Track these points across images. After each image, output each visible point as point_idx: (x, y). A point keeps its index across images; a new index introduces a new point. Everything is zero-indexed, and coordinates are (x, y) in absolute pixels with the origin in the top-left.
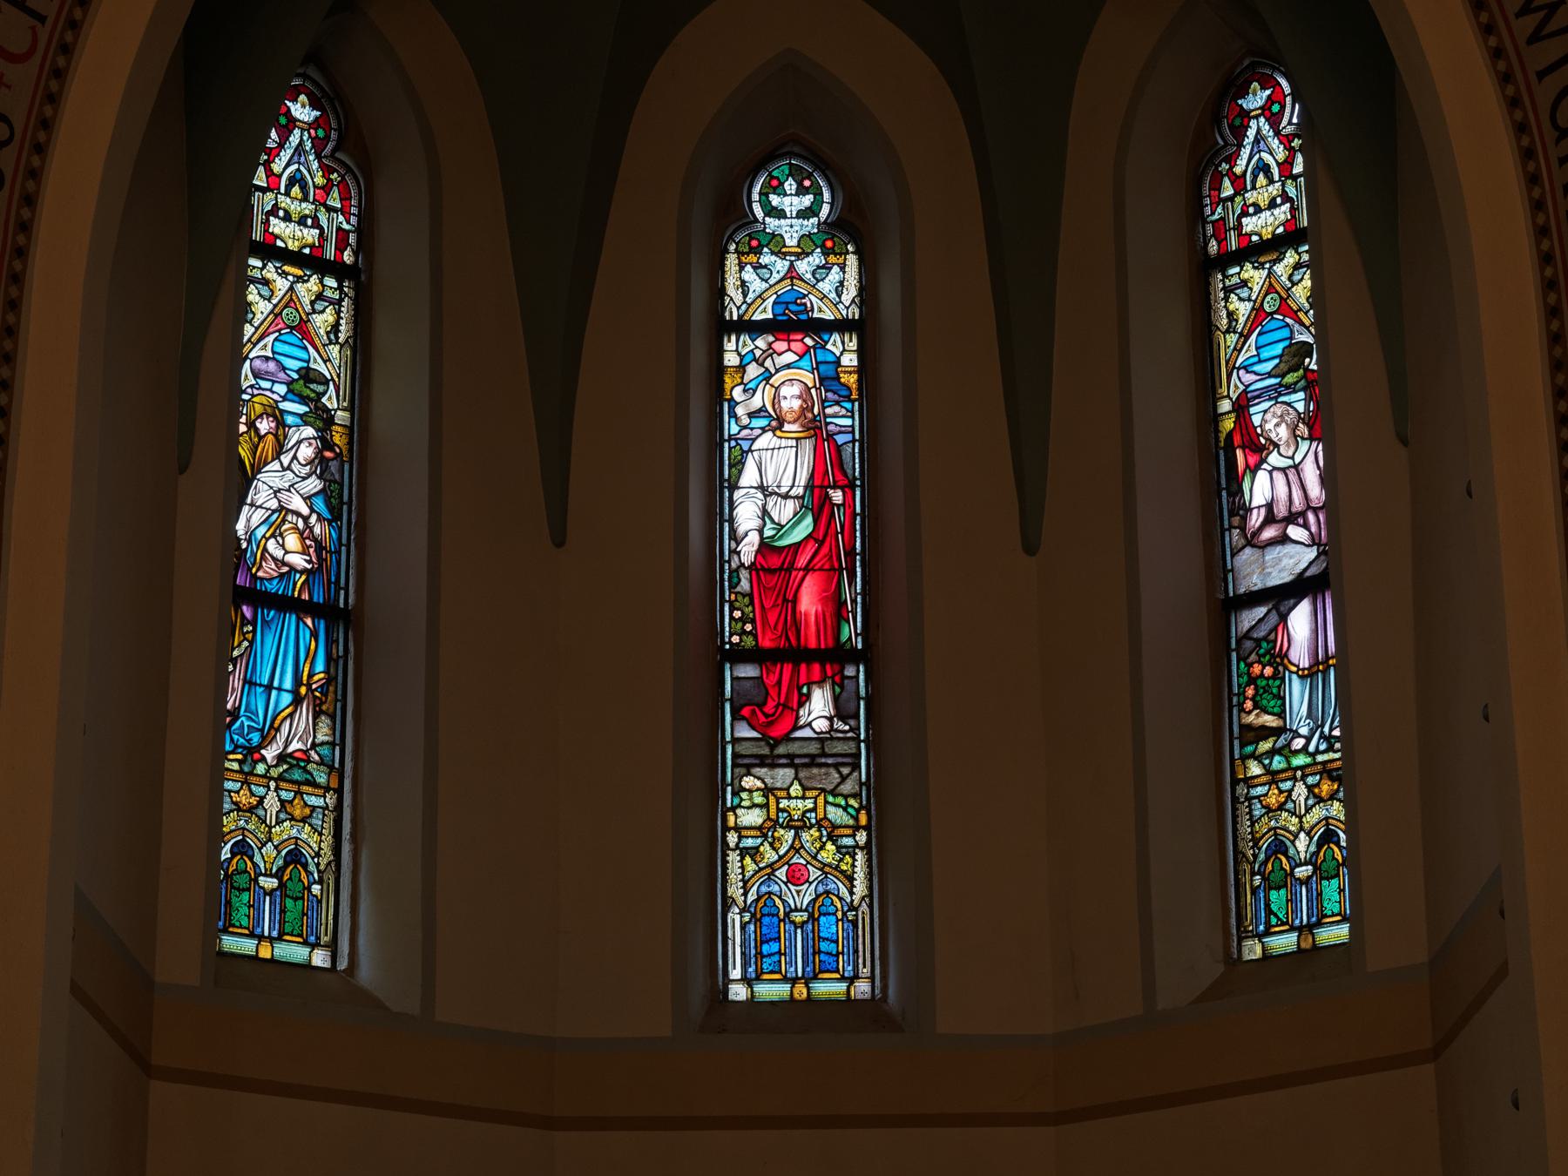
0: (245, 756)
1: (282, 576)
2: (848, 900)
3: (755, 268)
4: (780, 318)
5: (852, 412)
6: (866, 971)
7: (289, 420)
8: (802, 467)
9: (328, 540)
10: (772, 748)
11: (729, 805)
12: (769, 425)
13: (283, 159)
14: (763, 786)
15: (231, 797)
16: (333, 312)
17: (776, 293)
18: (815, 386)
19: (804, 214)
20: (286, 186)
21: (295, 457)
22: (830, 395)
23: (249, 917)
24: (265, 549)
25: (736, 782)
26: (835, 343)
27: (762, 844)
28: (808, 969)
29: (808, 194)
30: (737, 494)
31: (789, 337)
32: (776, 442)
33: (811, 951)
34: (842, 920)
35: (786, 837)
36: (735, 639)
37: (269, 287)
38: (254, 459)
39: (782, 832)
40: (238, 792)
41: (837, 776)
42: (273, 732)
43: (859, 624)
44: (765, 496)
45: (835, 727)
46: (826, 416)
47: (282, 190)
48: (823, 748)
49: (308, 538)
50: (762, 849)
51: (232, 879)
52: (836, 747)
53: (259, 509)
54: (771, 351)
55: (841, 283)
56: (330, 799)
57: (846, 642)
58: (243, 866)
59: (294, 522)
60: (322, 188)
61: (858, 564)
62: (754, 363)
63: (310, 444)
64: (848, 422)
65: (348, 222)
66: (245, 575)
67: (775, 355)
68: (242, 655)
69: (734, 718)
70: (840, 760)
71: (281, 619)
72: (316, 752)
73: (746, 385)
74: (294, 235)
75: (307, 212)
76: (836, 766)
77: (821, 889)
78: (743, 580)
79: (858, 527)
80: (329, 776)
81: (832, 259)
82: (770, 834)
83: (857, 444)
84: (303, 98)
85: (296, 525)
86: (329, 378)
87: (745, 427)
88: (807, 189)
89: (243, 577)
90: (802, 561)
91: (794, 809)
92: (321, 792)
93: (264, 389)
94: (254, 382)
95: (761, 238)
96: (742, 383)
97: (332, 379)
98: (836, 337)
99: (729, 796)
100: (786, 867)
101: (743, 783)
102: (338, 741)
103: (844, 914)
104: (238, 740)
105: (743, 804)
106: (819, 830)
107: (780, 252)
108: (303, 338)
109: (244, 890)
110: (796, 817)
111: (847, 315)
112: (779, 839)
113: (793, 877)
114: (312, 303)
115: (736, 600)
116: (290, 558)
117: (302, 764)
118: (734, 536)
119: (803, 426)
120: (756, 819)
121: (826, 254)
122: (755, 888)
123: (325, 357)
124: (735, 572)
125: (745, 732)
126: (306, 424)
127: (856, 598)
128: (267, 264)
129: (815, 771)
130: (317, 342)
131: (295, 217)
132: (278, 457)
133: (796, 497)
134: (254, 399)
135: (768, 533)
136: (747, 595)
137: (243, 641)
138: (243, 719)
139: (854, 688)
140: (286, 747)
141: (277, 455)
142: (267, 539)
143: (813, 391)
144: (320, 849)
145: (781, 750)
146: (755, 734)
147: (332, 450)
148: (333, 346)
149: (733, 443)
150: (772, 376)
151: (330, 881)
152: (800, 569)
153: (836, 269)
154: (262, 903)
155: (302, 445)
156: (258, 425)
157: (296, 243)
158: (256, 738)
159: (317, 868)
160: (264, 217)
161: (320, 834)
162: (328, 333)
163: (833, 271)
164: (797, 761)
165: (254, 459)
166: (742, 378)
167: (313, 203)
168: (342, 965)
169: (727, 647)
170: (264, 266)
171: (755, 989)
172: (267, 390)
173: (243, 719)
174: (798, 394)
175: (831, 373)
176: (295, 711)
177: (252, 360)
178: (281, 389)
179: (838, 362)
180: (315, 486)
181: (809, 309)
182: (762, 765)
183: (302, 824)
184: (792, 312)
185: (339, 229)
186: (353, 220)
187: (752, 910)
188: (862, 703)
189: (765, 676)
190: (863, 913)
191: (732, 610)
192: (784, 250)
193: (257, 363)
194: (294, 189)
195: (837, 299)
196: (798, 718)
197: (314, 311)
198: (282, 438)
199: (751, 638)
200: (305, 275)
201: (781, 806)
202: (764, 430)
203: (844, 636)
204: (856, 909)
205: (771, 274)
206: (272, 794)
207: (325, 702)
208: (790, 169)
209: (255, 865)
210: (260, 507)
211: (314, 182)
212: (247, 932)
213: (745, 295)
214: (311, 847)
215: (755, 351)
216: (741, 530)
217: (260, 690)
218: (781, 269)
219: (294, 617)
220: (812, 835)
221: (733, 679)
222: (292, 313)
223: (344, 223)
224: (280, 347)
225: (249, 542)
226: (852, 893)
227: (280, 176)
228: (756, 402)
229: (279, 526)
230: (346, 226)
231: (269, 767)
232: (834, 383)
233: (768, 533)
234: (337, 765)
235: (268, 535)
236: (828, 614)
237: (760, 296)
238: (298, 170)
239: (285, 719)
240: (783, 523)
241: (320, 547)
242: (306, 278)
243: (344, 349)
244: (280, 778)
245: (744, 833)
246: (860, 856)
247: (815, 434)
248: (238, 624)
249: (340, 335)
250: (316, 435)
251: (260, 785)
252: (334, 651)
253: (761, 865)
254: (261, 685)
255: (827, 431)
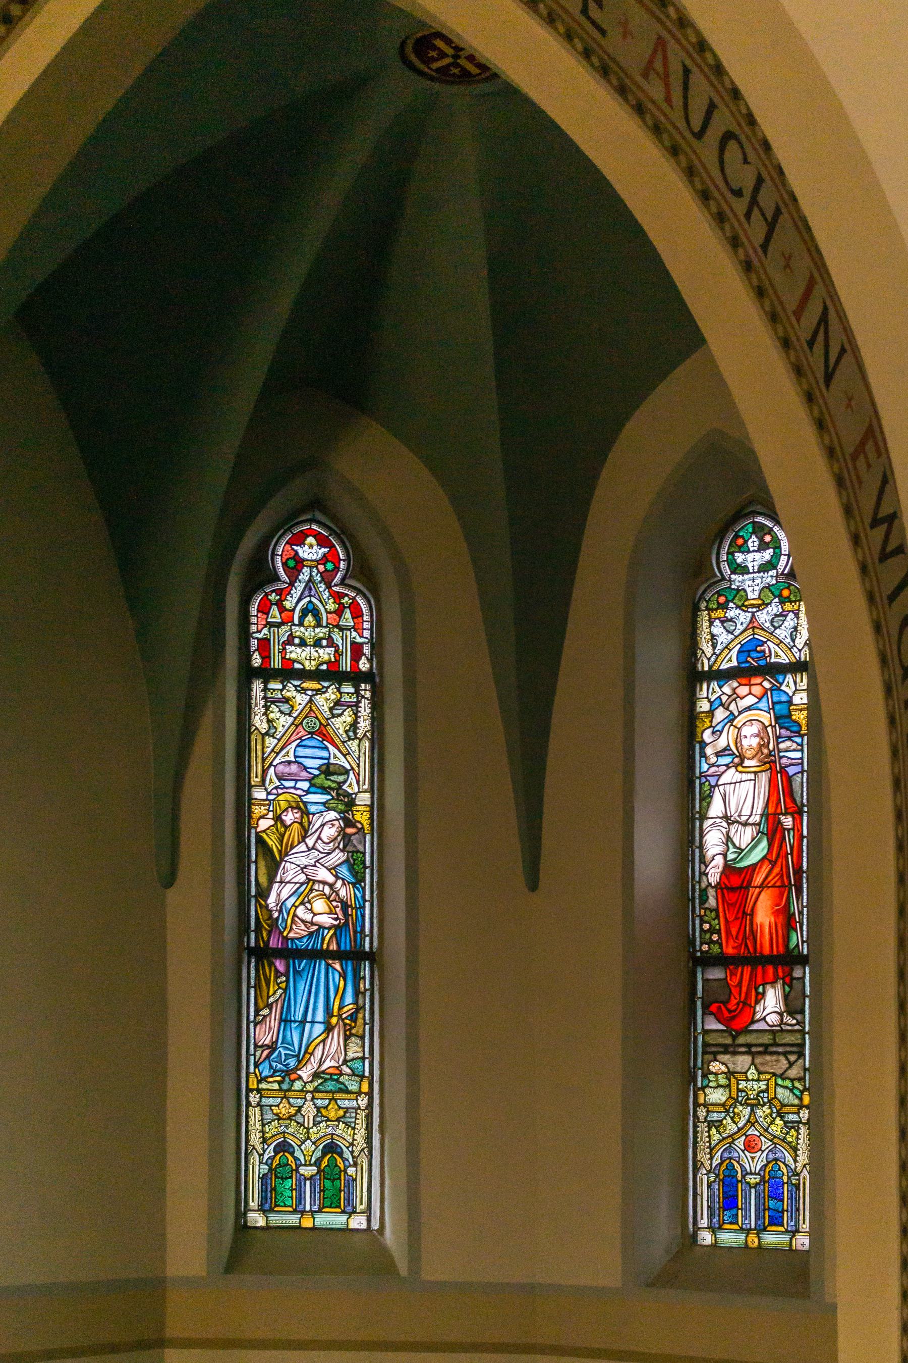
0: (283, 1078)
1: (311, 934)
2: (793, 1167)
3: (722, 622)
4: (743, 665)
5: (802, 745)
6: (806, 1227)
7: (313, 809)
8: (759, 798)
9: (353, 899)
10: (734, 1038)
11: (699, 1085)
12: (732, 762)
13: (294, 595)
14: (726, 1070)
15: (272, 1110)
16: (351, 713)
17: (740, 643)
18: (771, 725)
19: (765, 568)
20: (300, 618)
21: (319, 838)
22: (783, 732)
23: (292, 1198)
24: (295, 915)
25: (705, 1066)
26: (789, 684)
27: (725, 1118)
28: (759, 1222)
29: (769, 548)
30: (707, 823)
31: (750, 681)
32: (738, 777)
33: (762, 1207)
34: (787, 1183)
35: (744, 1112)
36: (705, 947)
37: (289, 703)
38: (282, 847)
39: (741, 1108)
40: (278, 1106)
41: (785, 1062)
42: (308, 1056)
43: (805, 933)
44: (729, 824)
45: (785, 1020)
46: (779, 751)
47: (296, 621)
48: (774, 1039)
49: (335, 900)
50: (724, 1122)
51: (276, 1171)
52: (785, 1038)
53: (288, 885)
54: (735, 696)
55: (795, 628)
56: (363, 1102)
57: (794, 948)
58: (285, 1161)
59: (321, 889)
60: (335, 612)
61: (804, 880)
62: (721, 707)
63: (333, 825)
64: (798, 755)
65: (361, 636)
66: (277, 937)
67: (738, 699)
68: (277, 1001)
69: (704, 1014)
70: (788, 1049)
71: (311, 969)
72: (348, 1066)
73: (714, 727)
74: (310, 657)
75: (321, 635)
76: (785, 1054)
77: (771, 1156)
78: (711, 898)
79: (805, 848)
80: (360, 1084)
81: (788, 607)
82: (731, 1109)
83: (805, 774)
84: (310, 540)
85: (323, 891)
86: (349, 767)
87: (713, 765)
88: (767, 544)
89: (276, 940)
90: (758, 880)
91: (751, 1090)
92: (353, 1096)
93: (287, 788)
94: (278, 784)
95: (728, 595)
96: (711, 726)
97: (352, 769)
98: (789, 678)
99: (699, 1078)
100: (744, 1137)
101: (710, 1067)
102: (367, 1055)
103: (789, 1178)
104: (276, 1066)
105: (711, 1084)
106: (770, 1108)
107: (743, 605)
108: (324, 740)
109: (287, 1178)
110: (752, 1096)
111: (800, 658)
112: (738, 1114)
113: (749, 1146)
114: (331, 709)
115: (705, 915)
116: (318, 919)
117: (335, 1077)
118: (703, 860)
119: (760, 761)
120: (721, 1097)
121: (782, 603)
122: (719, 1154)
123: (345, 752)
124: (704, 892)
125: (713, 1025)
126: (329, 809)
127: (803, 910)
128: (286, 685)
129: (768, 1058)
130: (337, 741)
131: (310, 641)
132: (304, 840)
133: (754, 824)
134: (280, 798)
135: (731, 856)
136: (714, 910)
137: (277, 990)
138: (281, 1049)
139: (801, 987)
140: (320, 1066)
141: (303, 839)
142: (297, 907)
143: (769, 729)
144: (354, 1140)
145: (741, 1040)
146: (721, 1027)
147: (354, 826)
148: (351, 741)
149: (704, 780)
150: (736, 717)
151: (364, 1164)
152: (756, 887)
153: (791, 615)
154: (302, 1186)
155: (325, 827)
156: (284, 817)
157: (313, 663)
158: (292, 1062)
159: (352, 1155)
160: (280, 647)
161: (354, 1129)
162: (346, 732)
163: (788, 618)
164: (754, 1049)
165: (282, 847)
166: (711, 722)
167: (326, 627)
168: (375, 1225)
169: (699, 954)
170: (284, 687)
171: (718, 1236)
172: (291, 788)
173: (281, 1049)
174: (757, 732)
175: (785, 712)
176: (328, 1037)
177: (275, 766)
178: (305, 785)
179: (790, 702)
180: (339, 859)
181: (767, 655)
182: (725, 1052)
183: (337, 1123)
184: (753, 659)
185: (353, 644)
186: (367, 634)
187: (717, 1171)
188: (807, 1000)
189: (729, 978)
190: (804, 1178)
191: (702, 922)
192: (746, 603)
193: (281, 768)
194: (307, 619)
195: (792, 644)
196: (754, 1013)
197: (333, 716)
198: (306, 824)
199: (717, 946)
200: (324, 687)
201: (740, 1087)
202: (728, 766)
203: (793, 944)
204: (798, 1175)
205: (736, 626)
206: (309, 1104)
207: (355, 1027)
208: (754, 528)
209: (296, 1159)
210: (289, 882)
211: (326, 609)
212: (290, 1209)
213: (714, 647)
214: (345, 1140)
215: (722, 697)
216: (709, 855)
217: (294, 1025)
218: (744, 621)
219: (323, 963)
220: (764, 1112)
221: (705, 981)
222: (312, 721)
223: (358, 637)
224: (301, 752)
225: (281, 911)
226: (795, 1161)
227: (293, 610)
228: (722, 743)
229: (308, 895)
230: (359, 640)
231: (305, 1083)
232: (787, 720)
233: (731, 856)
234: (367, 1074)
235: (297, 904)
236: (779, 926)
237: (726, 647)
238: (310, 602)
239: (319, 1044)
240: (743, 847)
241: (345, 906)
242: (324, 690)
243: (363, 742)
244: (316, 1090)
245: (711, 1108)
246: (803, 1130)
247: (770, 768)
248: (272, 978)
249: (358, 731)
250: (339, 817)
251: (298, 1098)
252: (362, 986)
253: (724, 1135)
254: (295, 1021)
255: (780, 764)
